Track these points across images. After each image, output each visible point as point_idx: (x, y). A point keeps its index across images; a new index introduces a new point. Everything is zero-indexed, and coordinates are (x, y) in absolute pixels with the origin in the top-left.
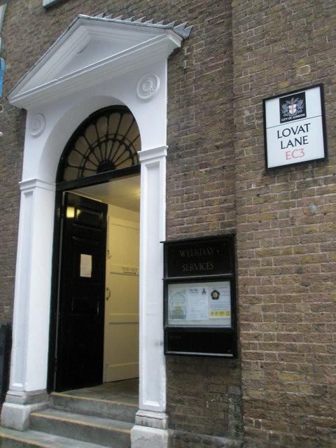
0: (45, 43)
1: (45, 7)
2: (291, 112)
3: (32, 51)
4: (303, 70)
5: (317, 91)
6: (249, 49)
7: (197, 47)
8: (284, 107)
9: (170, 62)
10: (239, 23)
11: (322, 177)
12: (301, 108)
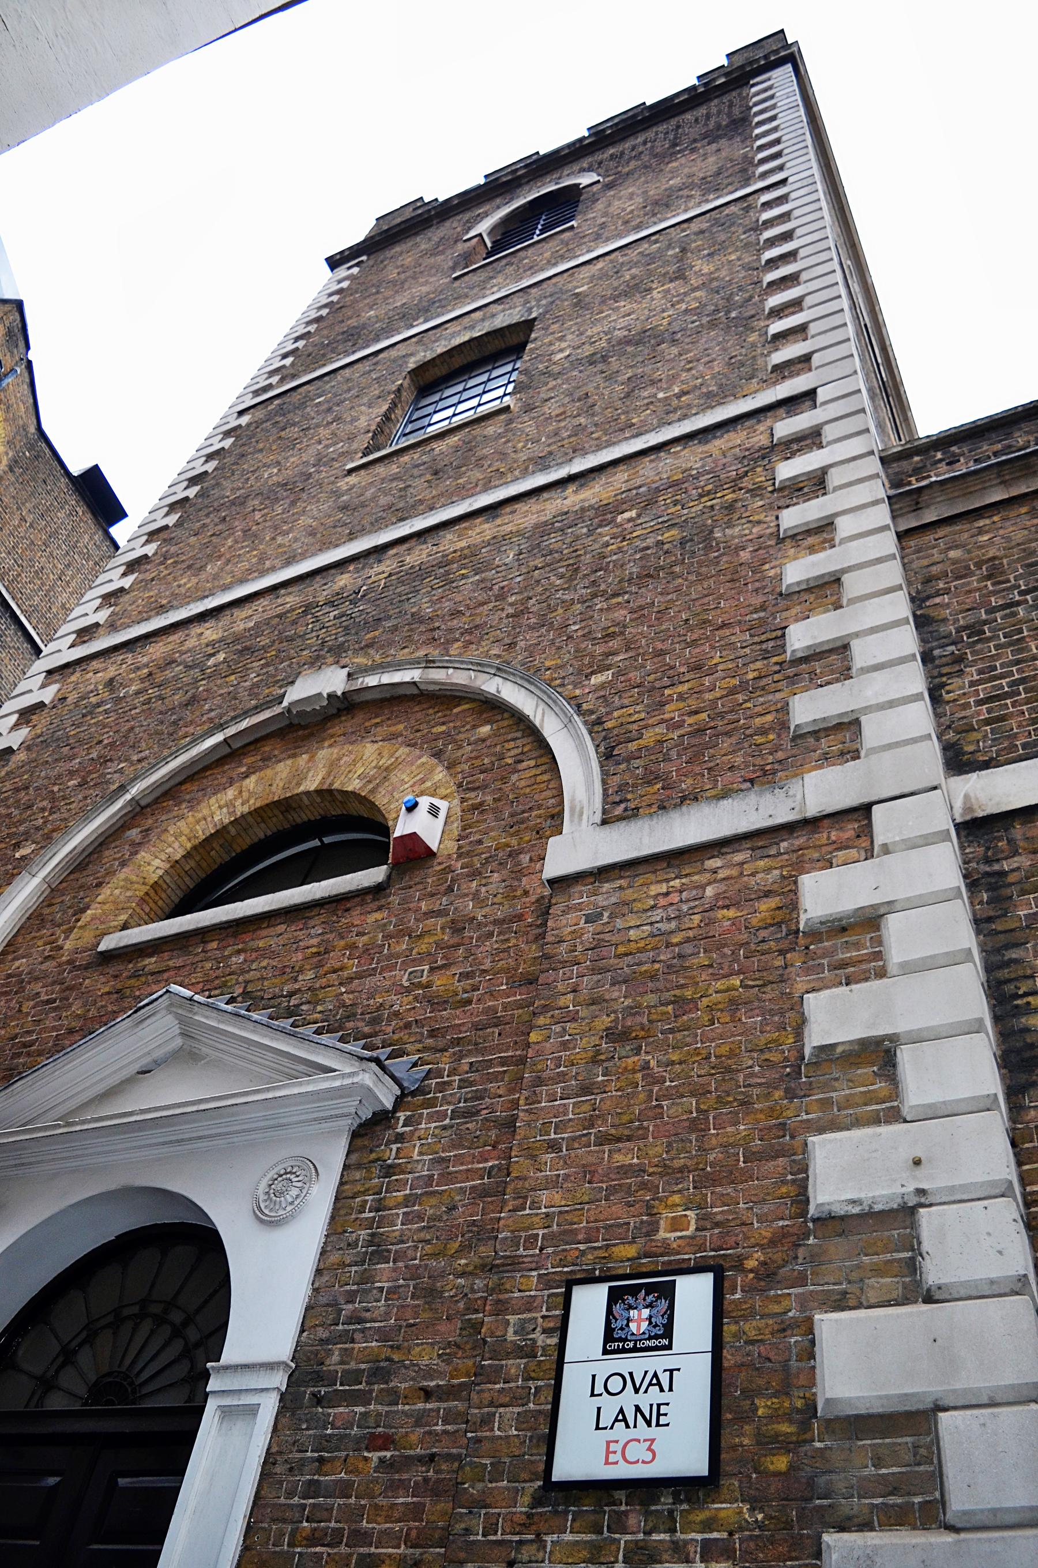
0: (71, 1031)
1: (101, 953)
2: (633, 1326)
3: (31, 1044)
4: (676, 1225)
5: (705, 1282)
6: (553, 1146)
7: (431, 1118)
8: (617, 1309)
9: (359, 1142)
10: (539, 1082)
11: (699, 1537)
12: (659, 1320)
